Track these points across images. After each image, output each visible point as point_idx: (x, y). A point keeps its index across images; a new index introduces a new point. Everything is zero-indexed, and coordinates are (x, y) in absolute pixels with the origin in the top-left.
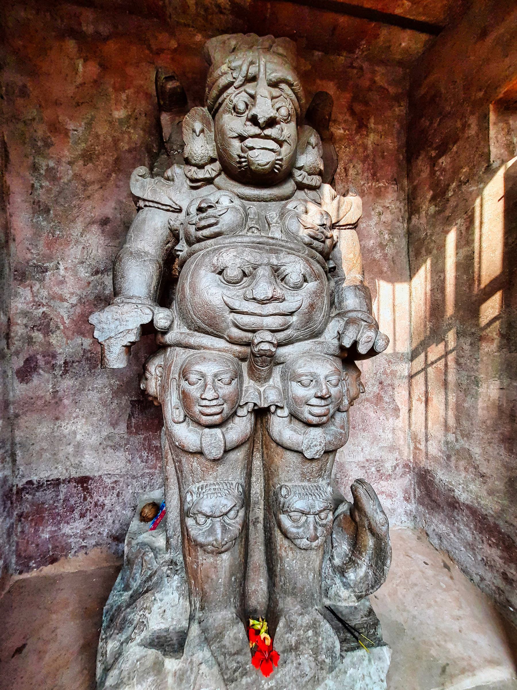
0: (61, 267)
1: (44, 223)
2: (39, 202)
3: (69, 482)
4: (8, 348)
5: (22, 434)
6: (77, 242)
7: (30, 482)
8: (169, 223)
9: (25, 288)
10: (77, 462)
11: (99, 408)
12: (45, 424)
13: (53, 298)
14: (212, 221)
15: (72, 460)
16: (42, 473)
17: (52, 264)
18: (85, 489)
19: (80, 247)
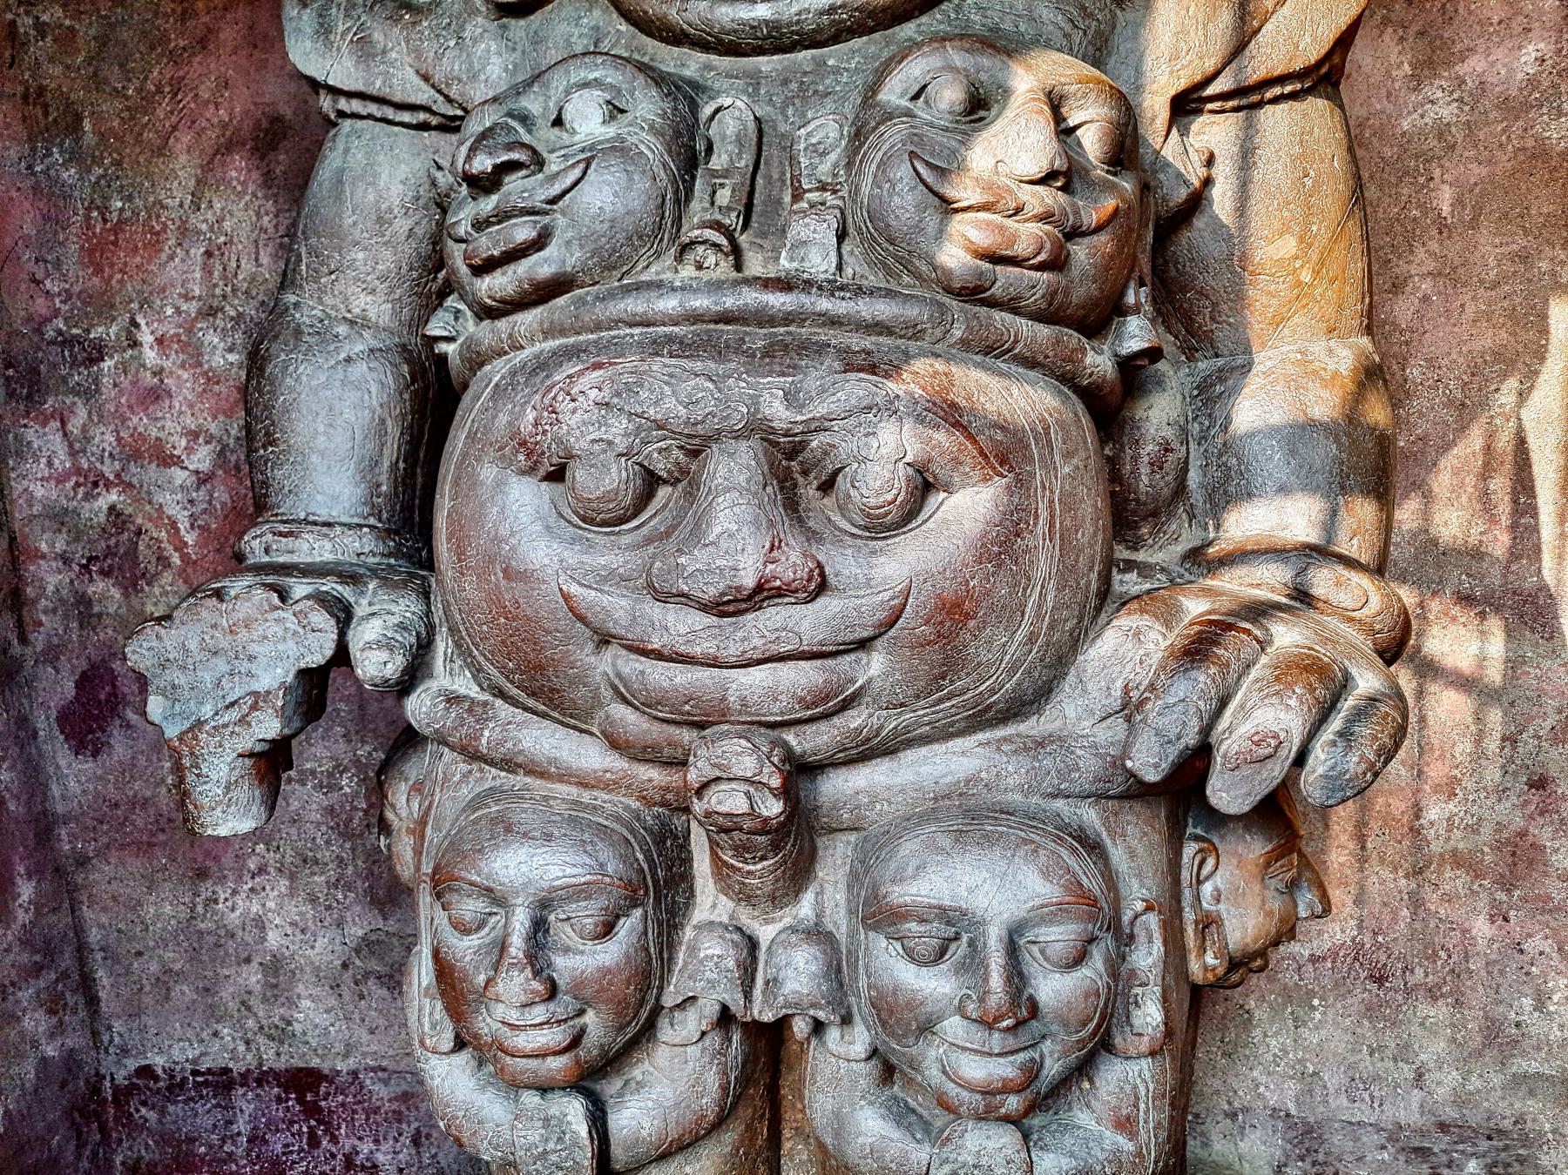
0: (146, 338)
1: (69, 174)
2: (41, 90)
3: (260, 1082)
4: (23, 640)
5: (104, 919)
6: (184, 231)
7: (146, 1072)
8: (434, 184)
9: (44, 425)
10: (276, 1020)
11: (328, 842)
12: (166, 889)
13: (136, 456)
14: (523, 232)
15: (261, 1014)
16: (174, 1050)
17: (114, 329)
18: (312, 1110)
19: (198, 252)
